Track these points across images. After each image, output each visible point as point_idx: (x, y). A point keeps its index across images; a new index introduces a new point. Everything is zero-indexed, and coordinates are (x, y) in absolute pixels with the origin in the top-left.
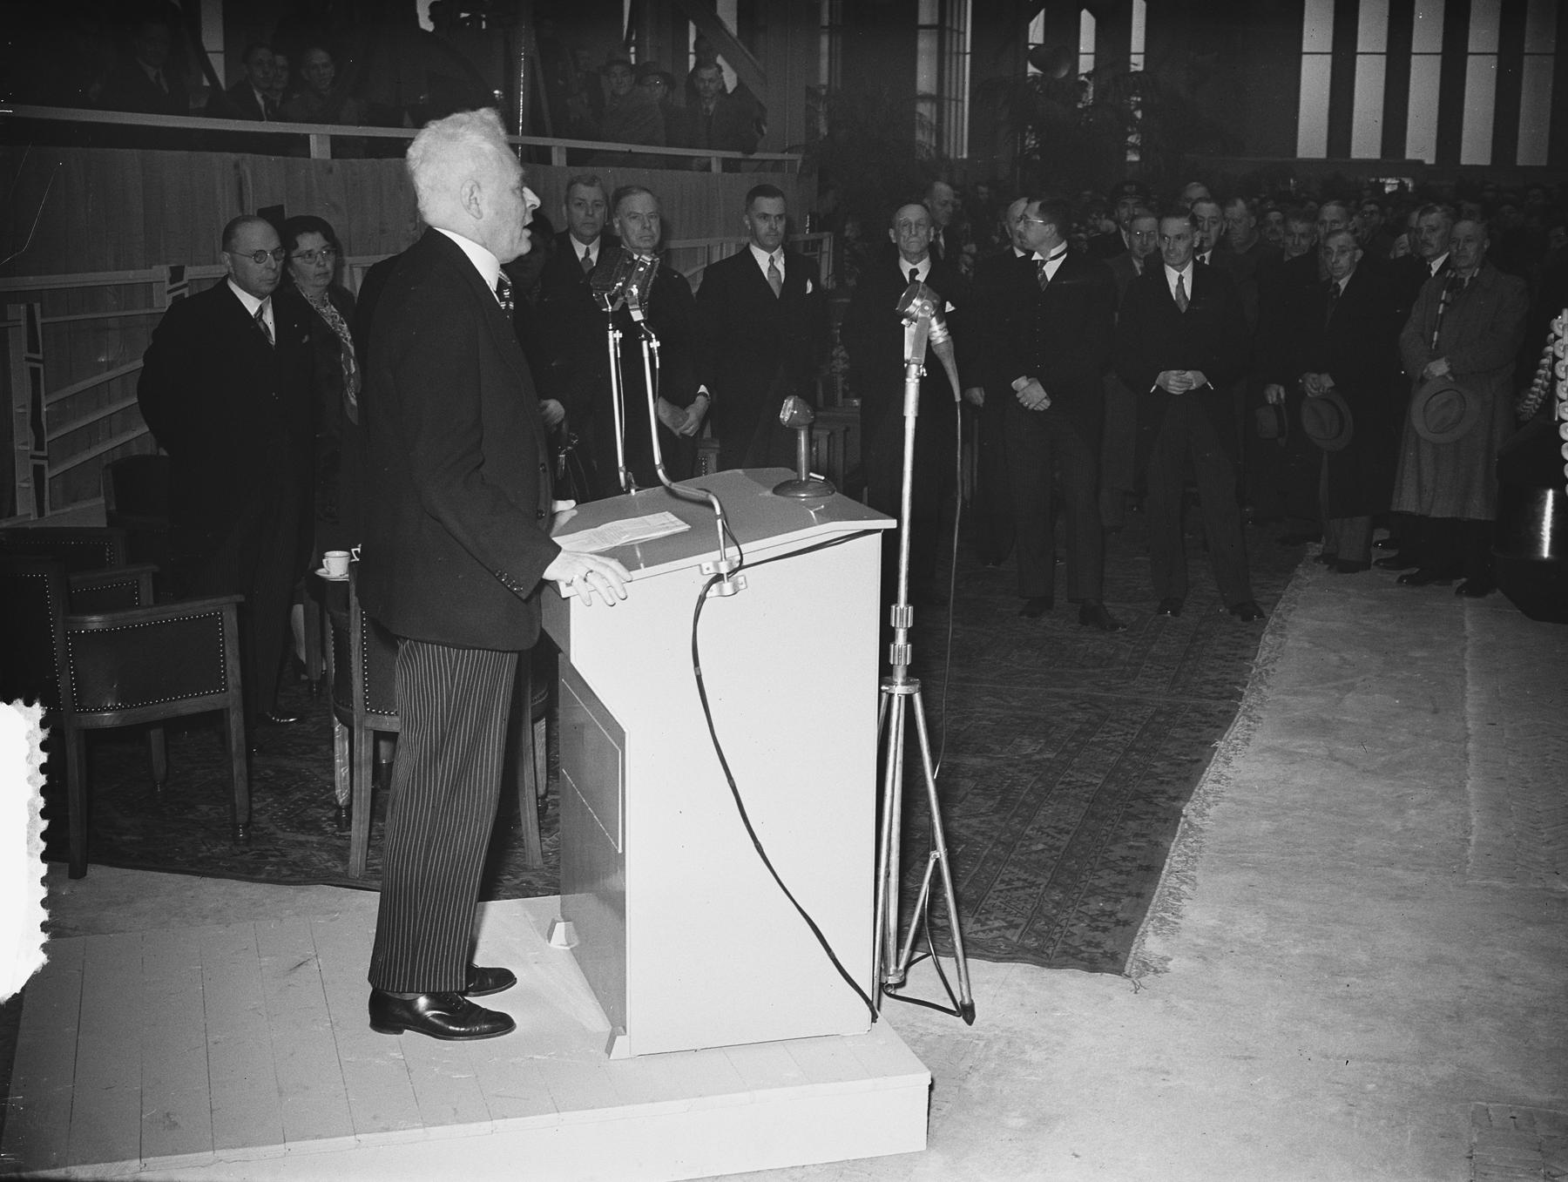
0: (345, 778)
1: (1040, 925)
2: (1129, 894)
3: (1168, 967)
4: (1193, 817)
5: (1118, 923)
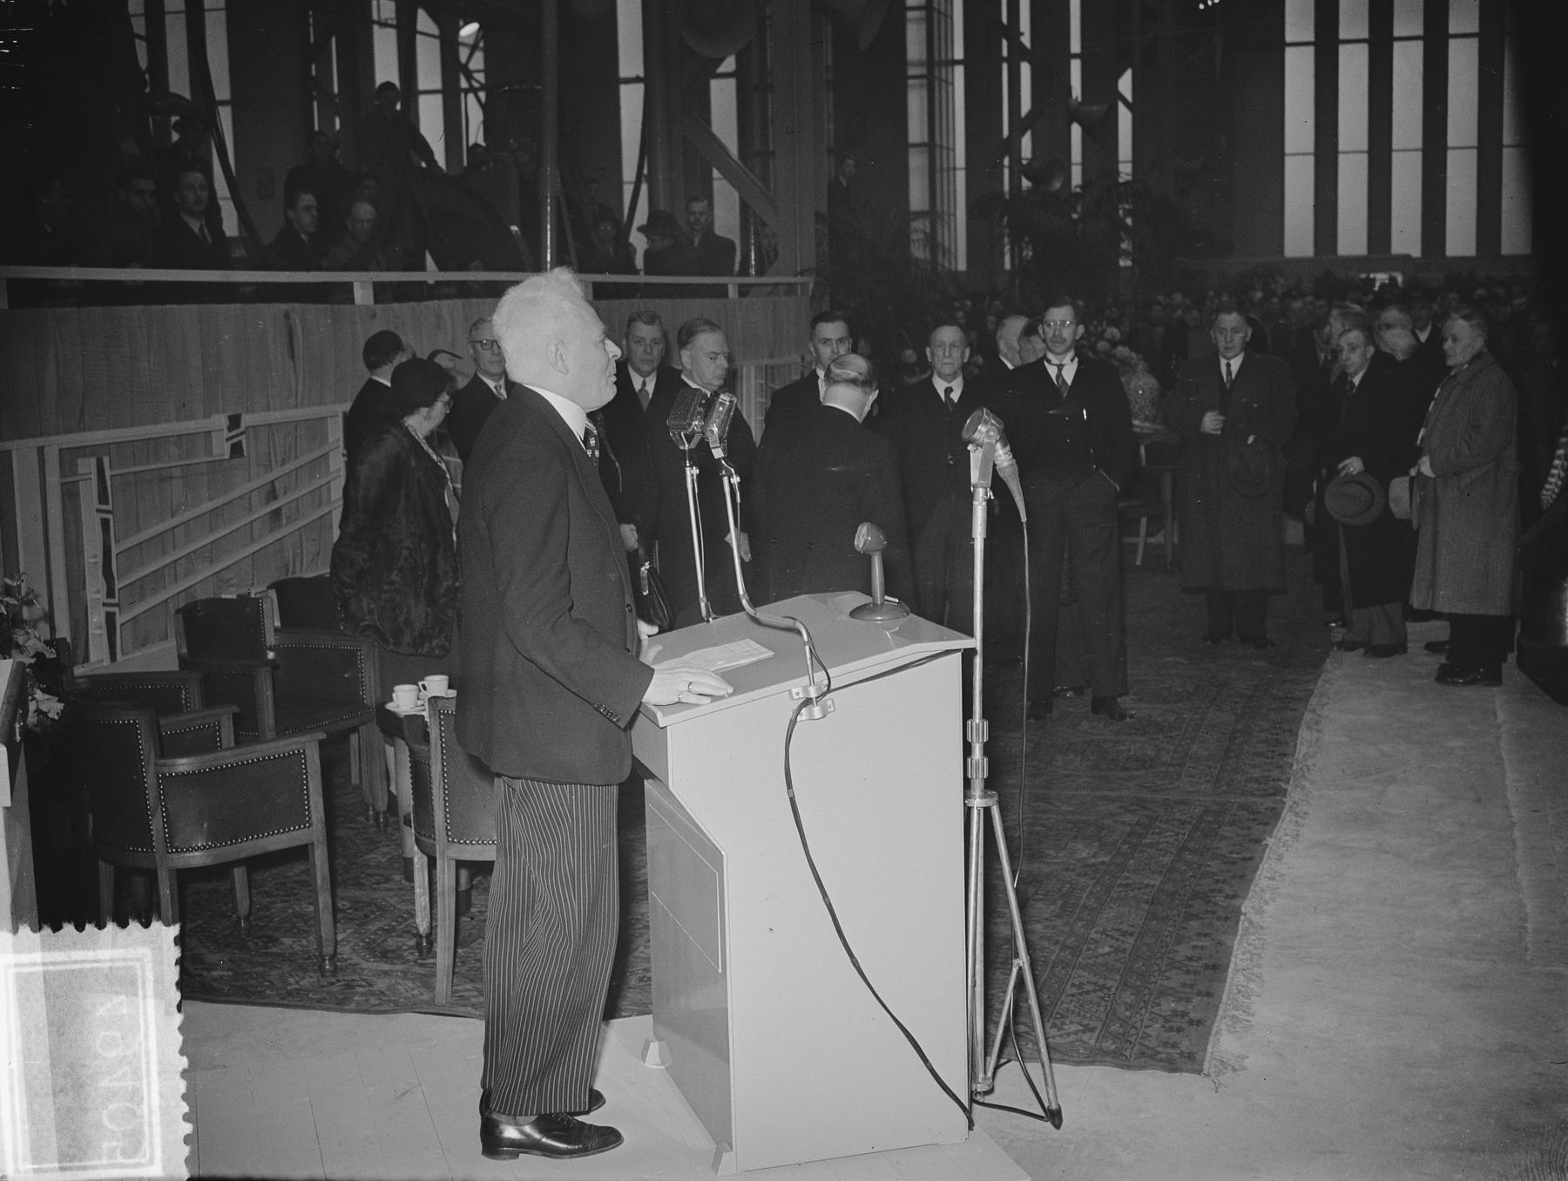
0: (425, 906)
1: (1115, 1028)
2: (1199, 994)
3: (1245, 1064)
4: (1252, 915)
5: (1191, 1022)
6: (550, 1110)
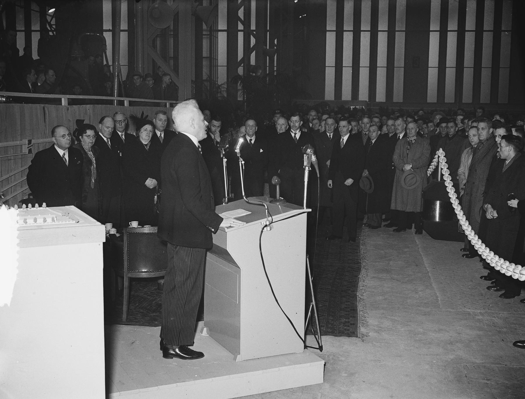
5: (351, 324)
6: (182, 344)
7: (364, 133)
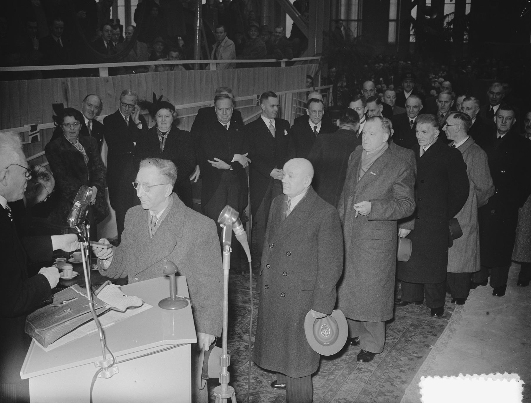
7: (441, 114)
